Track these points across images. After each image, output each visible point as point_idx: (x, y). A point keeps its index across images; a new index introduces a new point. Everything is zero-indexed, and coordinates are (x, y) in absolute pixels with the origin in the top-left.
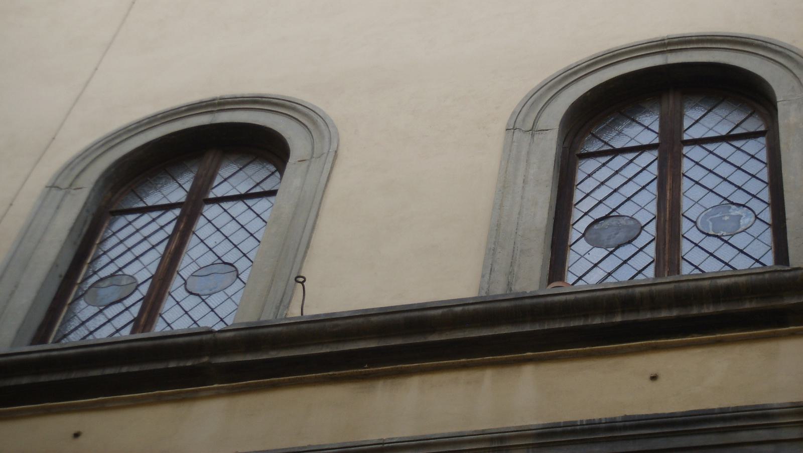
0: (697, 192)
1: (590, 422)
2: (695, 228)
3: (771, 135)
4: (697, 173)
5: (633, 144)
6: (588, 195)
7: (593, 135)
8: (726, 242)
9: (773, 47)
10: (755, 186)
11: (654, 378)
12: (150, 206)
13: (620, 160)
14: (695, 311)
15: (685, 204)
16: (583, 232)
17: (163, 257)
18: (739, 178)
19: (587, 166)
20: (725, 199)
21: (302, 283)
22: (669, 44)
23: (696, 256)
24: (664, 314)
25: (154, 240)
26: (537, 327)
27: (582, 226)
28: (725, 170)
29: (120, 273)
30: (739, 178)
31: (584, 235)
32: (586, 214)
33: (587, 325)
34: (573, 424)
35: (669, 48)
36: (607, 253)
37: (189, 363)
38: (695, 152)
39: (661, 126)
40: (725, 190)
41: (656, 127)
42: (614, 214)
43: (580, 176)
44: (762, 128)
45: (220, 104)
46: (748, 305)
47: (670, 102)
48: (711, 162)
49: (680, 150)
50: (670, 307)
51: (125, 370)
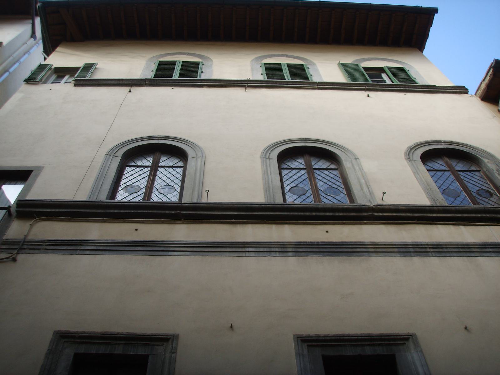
0: (160, 181)
1: (311, 242)
2: (157, 191)
3: (184, 167)
4: (319, 178)
5: (143, 165)
6: (127, 178)
7: (284, 163)
8: (165, 196)
9: (338, 145)
10: (177, 181)
11: (327, 232)
12: (139, 166)
13: (138, 169)
14: (337, 214)
15: (156, 184)
16: (289, 190)
17: (148, 181)
18: (173, 178)
19: (128, 169)
20: (330, 186)
21: (207, 192)
22: (305, 140)
23: (325, 200)
24: (328, 214)
25: (128, 175)
26: (289, 214)
27: (123, 186)
28: (169, 175)
29: (134, 184)
30: (173, 178)
31: (123, 189)
32: (125, 183)
33: (304, 215)
34: (306, 242)
35: (306, 141)
36: (298, 197)
37: (173, 212)
38: (161, 170)
39: (153, 161)
40: (168, 181)
41: (151, 161)
42: (297, 186)
43: (125, 172)
44: (183, 165)
45: (160, 138)
46: (352, 214)
47: (158, 154)
48: (166, 173)
49: (158, 169)
50: (329, 212)
51: (151, 212)
